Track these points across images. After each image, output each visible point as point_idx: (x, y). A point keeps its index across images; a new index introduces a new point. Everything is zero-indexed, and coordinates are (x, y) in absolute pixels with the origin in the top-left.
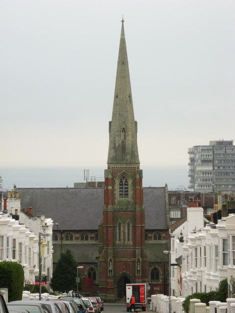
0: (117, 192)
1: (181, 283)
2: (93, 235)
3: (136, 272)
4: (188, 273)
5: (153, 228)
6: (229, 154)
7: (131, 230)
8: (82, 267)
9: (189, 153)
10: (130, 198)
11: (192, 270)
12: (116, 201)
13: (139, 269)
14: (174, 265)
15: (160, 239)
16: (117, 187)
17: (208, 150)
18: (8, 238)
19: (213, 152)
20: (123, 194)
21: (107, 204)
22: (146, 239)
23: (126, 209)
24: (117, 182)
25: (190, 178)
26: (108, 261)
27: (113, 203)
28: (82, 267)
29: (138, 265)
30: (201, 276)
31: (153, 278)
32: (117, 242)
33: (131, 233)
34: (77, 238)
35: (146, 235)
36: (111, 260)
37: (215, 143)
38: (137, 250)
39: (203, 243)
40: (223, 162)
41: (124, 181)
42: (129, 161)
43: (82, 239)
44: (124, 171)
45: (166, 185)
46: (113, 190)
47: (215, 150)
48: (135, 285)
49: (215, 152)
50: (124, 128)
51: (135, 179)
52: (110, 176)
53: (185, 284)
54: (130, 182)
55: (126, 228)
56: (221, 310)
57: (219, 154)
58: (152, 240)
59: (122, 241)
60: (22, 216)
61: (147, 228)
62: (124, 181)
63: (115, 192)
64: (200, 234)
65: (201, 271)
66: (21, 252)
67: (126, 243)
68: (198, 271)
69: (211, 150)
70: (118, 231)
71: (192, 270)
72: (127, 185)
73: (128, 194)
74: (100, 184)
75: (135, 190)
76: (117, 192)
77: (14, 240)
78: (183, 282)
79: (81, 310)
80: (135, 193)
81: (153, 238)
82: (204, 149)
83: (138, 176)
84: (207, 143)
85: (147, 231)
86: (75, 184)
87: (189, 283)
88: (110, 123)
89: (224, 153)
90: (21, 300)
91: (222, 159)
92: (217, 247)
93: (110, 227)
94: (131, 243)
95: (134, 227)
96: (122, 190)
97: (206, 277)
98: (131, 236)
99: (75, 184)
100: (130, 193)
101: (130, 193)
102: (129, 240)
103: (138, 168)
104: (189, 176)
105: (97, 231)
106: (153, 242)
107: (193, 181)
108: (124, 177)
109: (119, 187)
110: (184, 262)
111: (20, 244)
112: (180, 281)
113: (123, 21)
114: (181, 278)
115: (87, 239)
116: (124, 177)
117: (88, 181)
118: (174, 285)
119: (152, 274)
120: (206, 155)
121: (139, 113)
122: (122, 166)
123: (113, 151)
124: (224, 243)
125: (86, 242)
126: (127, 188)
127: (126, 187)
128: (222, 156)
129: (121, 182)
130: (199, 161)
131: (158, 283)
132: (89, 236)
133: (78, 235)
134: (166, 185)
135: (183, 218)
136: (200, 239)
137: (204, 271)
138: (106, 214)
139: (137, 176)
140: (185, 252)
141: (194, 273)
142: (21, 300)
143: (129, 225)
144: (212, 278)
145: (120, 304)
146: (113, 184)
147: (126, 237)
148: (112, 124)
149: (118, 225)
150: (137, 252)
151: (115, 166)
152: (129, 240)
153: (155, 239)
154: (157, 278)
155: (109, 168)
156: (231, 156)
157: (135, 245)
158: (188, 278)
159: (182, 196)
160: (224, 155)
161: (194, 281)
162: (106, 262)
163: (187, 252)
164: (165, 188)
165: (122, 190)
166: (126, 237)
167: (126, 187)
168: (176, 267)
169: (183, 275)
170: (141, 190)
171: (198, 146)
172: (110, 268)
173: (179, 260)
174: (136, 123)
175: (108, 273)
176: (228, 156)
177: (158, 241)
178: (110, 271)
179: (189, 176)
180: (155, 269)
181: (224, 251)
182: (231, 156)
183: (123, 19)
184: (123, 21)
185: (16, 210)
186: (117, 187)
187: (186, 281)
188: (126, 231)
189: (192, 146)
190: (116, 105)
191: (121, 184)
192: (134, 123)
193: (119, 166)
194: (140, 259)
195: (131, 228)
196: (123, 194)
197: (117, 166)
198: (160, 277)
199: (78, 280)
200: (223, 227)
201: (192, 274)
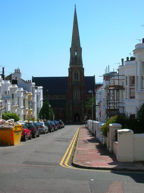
10: (79, 80)
12: (73, 81)
14: (97, 105)
31: (89, 113)
45: (94, 75)
48: (63, 156)
51: (81, 71)
67: (77, 98)
83: (82, 70)
86: (84, 68)
90: (143, 39)
94: (80, 98)
99: (84, 68)
100: (79, 77)
101: (79, 77)
102: (79, 98)
113: (75, 6)
119: (89, 112)
121: (83, 44)
134: (94, 75)
139: (82, 70)
142: (143, 39)
168: (98, 106)
174: (81, 48)
190: (73, 40)
192: (80, 49)
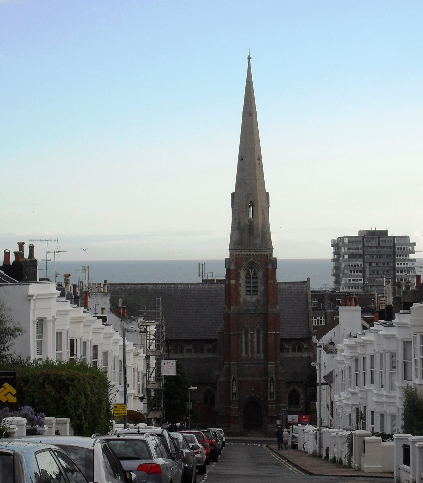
0: (242, 288)
1: (332, 409)
2: (210, 347)
3: (269, 395)
4: (343, 395)
5: (292, 337)
6: (384, 247)
7: (261, 340)
8: (196, 388)
9: (332, 245)
11: (350, 390)
12: (241, 300)
13: (272, 391)
15: (300, 350)
16: (242, 280)
17: (356, 242)
18: (85, 343)
19: (364, 244)
20: (250, 291)
21: (229, 303)
22: (282, 351)
23: (255, 310)
24: (243, 274)
25: (334, 277)
26: (231, 380)
27: (238, 303)
28: (196, 388)
29: (270, 385)
30: (366, 399)
32: (244, 355)
33: (261, 344)
34: (189, 351)
35: (282, 347)
36: (234, 379)
37: (365, 233)
38: (269, 366)
39: (369, 351)
40: (375, 257)
41: (252, 274)
42: (258, 246)
43: (196, 352)
44: (252, 259)
46: (238, 284)
47: (365, 242)
49: (366, 245)
50: (251, 202)
52: (233, 267)
53: (340, 411)
54: (260, 274)
55: (255, 336)
56: (419, 448)
57: (370, 248)
58: (289, 351)
59: (250, 354)
60: (111, 317)
61: (284, 335)
62: (252, 274)
63: (240, 288)
64: (364, 338)
65: (366, 391)
66: (96, 358)
68: (361, 391)
69: (360, 242)
70: (244, 340)
71: (350, 390)
72: (257, 278)
73: (257, 291)
74: (219, 281)
75: (266, 285)
76: (242, 288)
77: (95, 347)
78: (335, 407)
79: (127, 339)
80: (266, 291)
81: (291, 350)
82: (352, 240)
83: (270, 267)
84: (140, 460)
85: (283, 340)
87: (346, 409)
88: (233, 195)
89: (377, 245)
91: (375, 253)
92: (393, 356)
93: (234, 335)
94: (262, 355)
95: (266, 336)
96: (248, 285)
97: (375, 399)
98: (261, 348)
100: (261, 288)
101: (261, 288)
103: (271, 255)
104: (334, 275)
105: (215, 340)
106: (290, 355)
107: (337, 282)
108: (252, 268)
109: (244, 280)
110: (337, 381)
111: (105, 353)
112: (331, 407)
113: (249, 58)
114: (332, 403)
115: (202, 351)
116: (252, 265)
117: (204, 278)
118: (322, 412)
120: (355, 249)
122: (249, 253)
123: (236, 232)
124: (405, 351)
125: (201, 356)
126: (257, 282)
127: (255, 280)
128: (374, 249)
129: (248, 274)
130: (346, 257)
131: (298, 409)
132: (205, 348)
133: (190, 347)
134: (308, 280)
135: (333, 322)
136: (363, 345)
137: (371, 391)
138: (227, 317)
140: (339, 366)
141: (353, 394)
143: (258, 332)
144: (384, 399)
145: (247, 439)
146: (237, 277)
147: (255, 349)
148: (235, 196)
149: (243, 332)
150: (269, 369)
151: (240, 253)
152: (258, 352)
153: (294, 350)
154: (297, 403)
155: (231, 255)
156: (385, 249)
157: (266, 358)
158: (344, 402)
159: (326, 296)
160: (377, 248)
161: (353, 405)
162: (228, 382)
163: (343, 366)
164: (307, 283)
165: (248, 285)
166: (255, 349)
167: (255, 280)
169: (336, 397)
170: (276, 285)
171: (344, 237)
172: (234, 390)
173: (329, 379)
174: (267, 195)
175: (231, 397)
176: (382, 250)
177: (297, 353)
178: (233, 394)
179: (334, 275)
180: (294, 391)
181: (405, 359)
182: (385, 249)
183: (249, 56)
184: (249, 58)
185: (103, 309)
186: (242, 280)
187: (340, 406)
188: (255, 340)
189: (336, 238)
191: (248, 277)
193: (246, 253)
194: (274, 378)
195: (261, 335)
196: (250, 291)
197: (243, 253)
198: (301, 402)
199: (189, 406)
200: (392, 335)
201: (350, 396)
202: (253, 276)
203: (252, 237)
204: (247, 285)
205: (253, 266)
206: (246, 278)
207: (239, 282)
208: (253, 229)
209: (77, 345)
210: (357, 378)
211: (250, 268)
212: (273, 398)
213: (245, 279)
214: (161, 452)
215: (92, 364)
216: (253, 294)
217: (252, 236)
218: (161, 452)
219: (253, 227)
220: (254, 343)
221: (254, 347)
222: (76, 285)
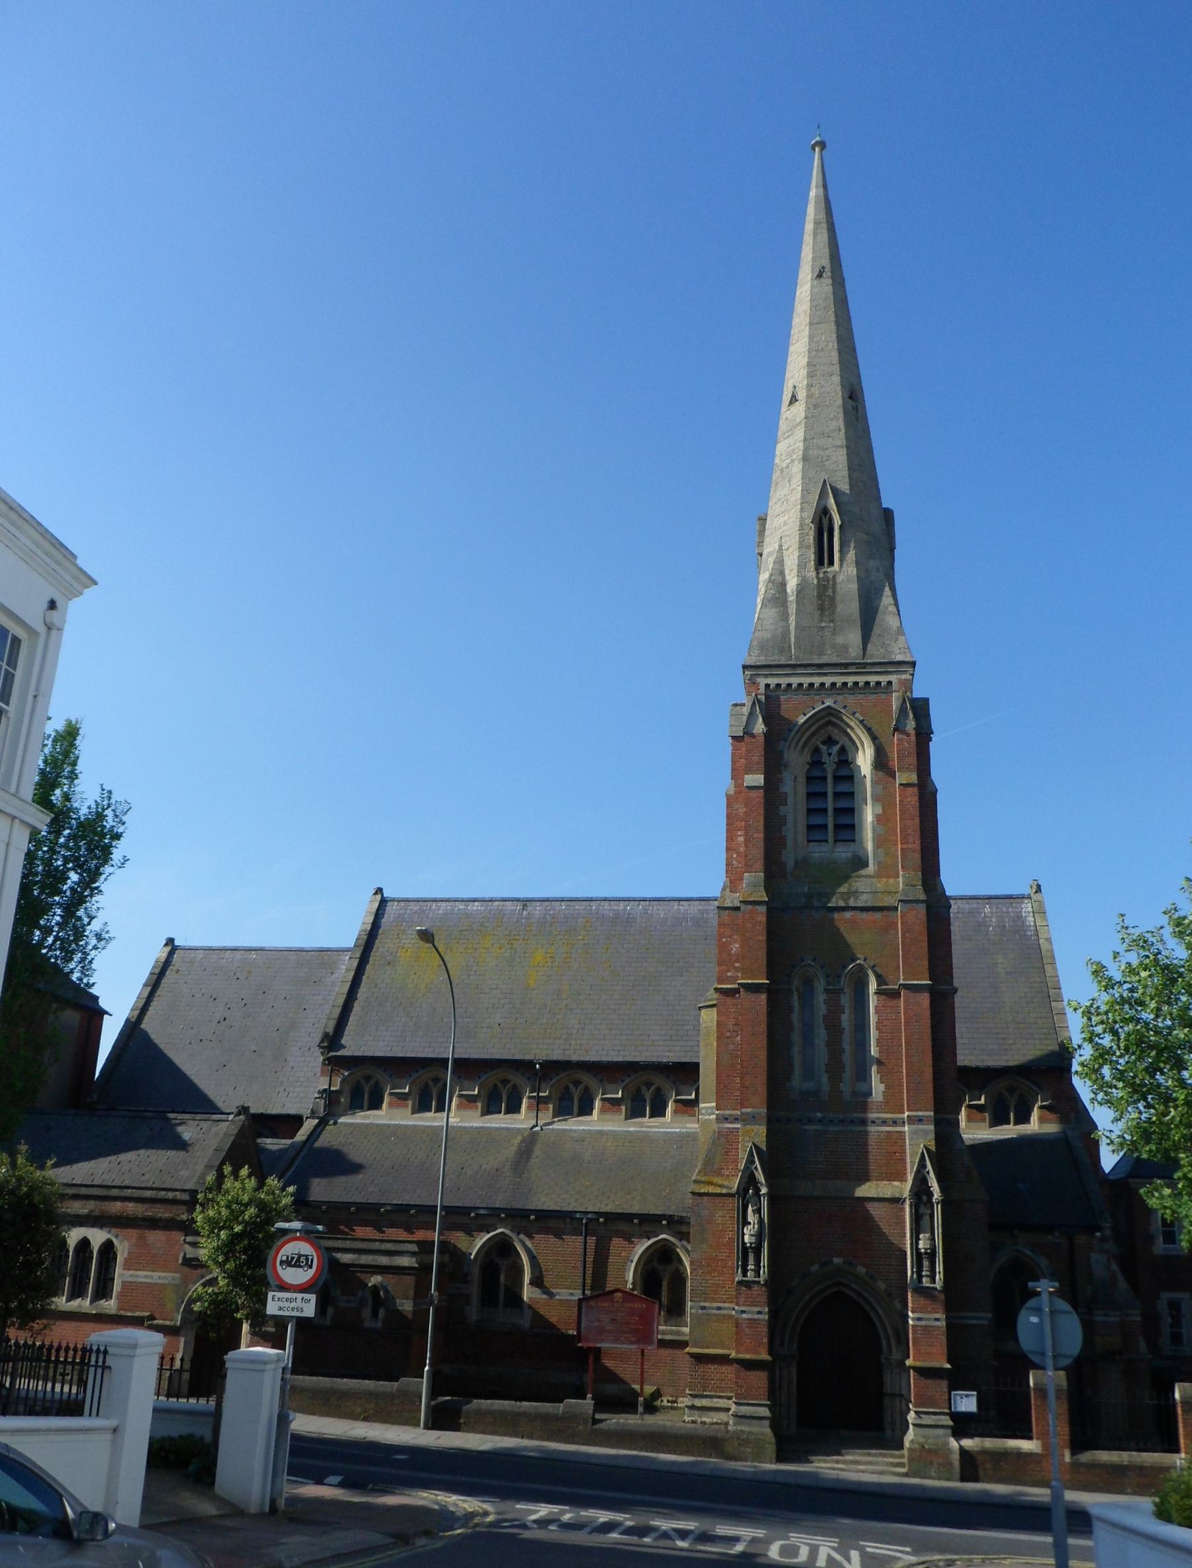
59: (825, 1080)
109: (802, 789)
174: (888, 515)
202: (836, 770)
203: (832, 624)
204: (812, 806)
205: (836, 737)
206: (810, 779)
207: (781, 790)
208: (832, 599)
209: (20, 776)
210: (75, 1430)
211: (824, 743)
212: (933, 1281)
213: (802, 780)
214: (642, 1364)
215: (656, 1315)
216: (836, 841)
217: (832, 621)
218: (642, 1364)
219: (834, 592)
220: (842, 1032)
221: (843, 1050)
222: (676, 1310)
